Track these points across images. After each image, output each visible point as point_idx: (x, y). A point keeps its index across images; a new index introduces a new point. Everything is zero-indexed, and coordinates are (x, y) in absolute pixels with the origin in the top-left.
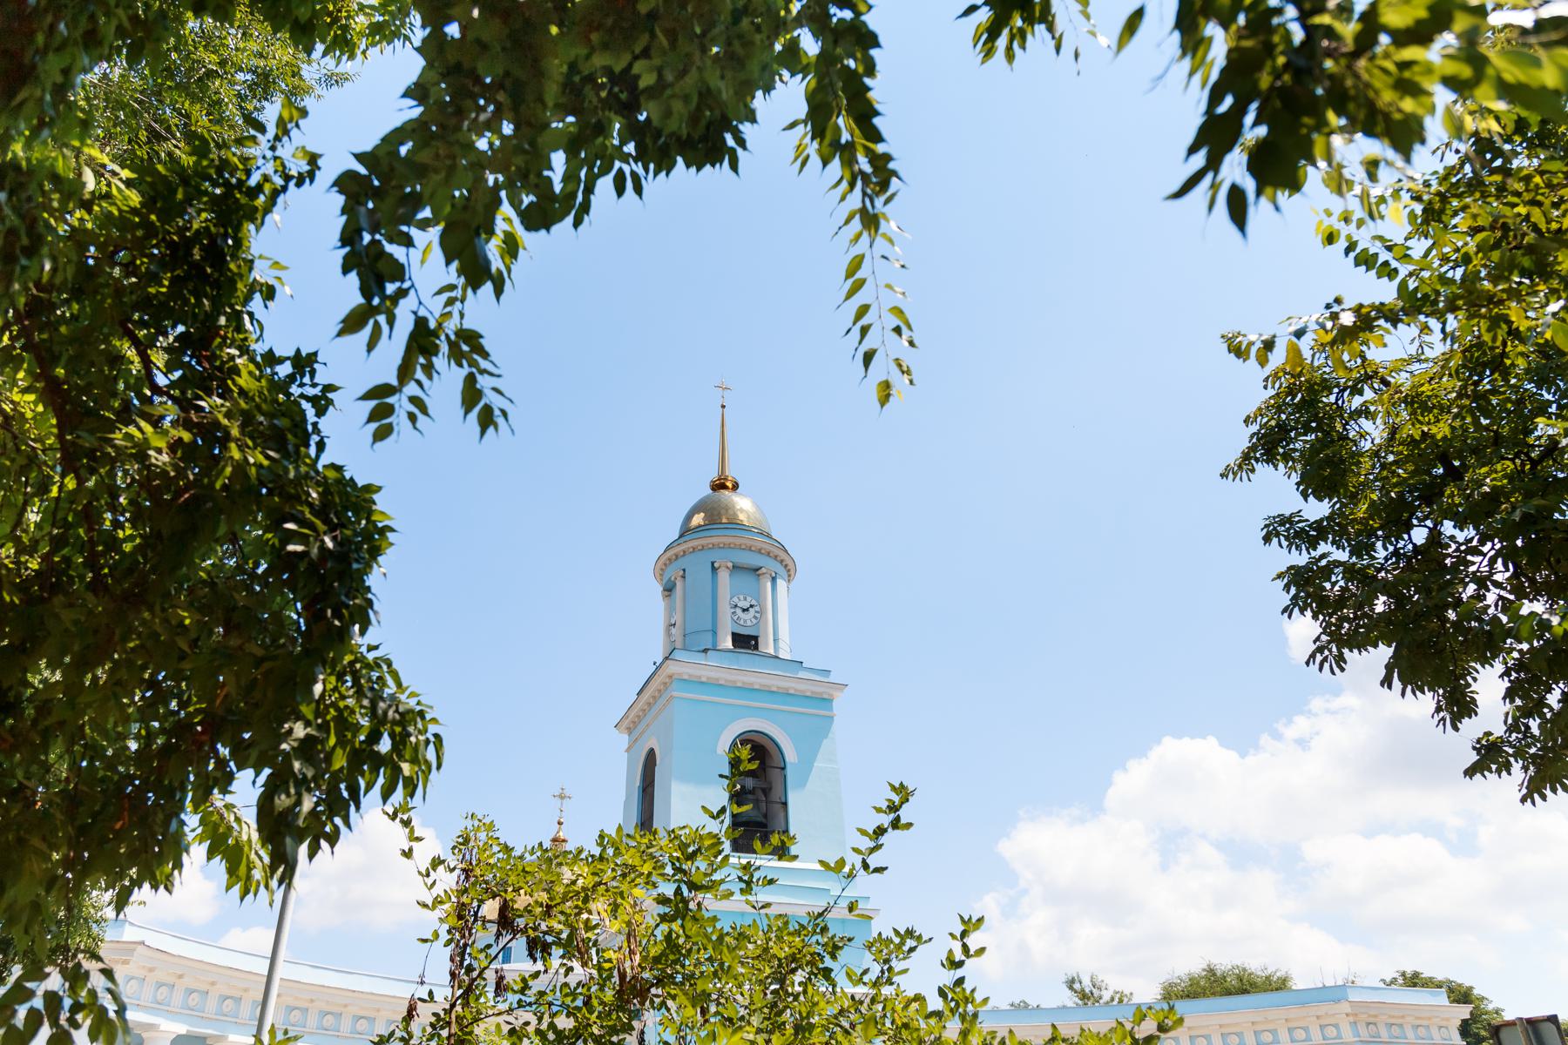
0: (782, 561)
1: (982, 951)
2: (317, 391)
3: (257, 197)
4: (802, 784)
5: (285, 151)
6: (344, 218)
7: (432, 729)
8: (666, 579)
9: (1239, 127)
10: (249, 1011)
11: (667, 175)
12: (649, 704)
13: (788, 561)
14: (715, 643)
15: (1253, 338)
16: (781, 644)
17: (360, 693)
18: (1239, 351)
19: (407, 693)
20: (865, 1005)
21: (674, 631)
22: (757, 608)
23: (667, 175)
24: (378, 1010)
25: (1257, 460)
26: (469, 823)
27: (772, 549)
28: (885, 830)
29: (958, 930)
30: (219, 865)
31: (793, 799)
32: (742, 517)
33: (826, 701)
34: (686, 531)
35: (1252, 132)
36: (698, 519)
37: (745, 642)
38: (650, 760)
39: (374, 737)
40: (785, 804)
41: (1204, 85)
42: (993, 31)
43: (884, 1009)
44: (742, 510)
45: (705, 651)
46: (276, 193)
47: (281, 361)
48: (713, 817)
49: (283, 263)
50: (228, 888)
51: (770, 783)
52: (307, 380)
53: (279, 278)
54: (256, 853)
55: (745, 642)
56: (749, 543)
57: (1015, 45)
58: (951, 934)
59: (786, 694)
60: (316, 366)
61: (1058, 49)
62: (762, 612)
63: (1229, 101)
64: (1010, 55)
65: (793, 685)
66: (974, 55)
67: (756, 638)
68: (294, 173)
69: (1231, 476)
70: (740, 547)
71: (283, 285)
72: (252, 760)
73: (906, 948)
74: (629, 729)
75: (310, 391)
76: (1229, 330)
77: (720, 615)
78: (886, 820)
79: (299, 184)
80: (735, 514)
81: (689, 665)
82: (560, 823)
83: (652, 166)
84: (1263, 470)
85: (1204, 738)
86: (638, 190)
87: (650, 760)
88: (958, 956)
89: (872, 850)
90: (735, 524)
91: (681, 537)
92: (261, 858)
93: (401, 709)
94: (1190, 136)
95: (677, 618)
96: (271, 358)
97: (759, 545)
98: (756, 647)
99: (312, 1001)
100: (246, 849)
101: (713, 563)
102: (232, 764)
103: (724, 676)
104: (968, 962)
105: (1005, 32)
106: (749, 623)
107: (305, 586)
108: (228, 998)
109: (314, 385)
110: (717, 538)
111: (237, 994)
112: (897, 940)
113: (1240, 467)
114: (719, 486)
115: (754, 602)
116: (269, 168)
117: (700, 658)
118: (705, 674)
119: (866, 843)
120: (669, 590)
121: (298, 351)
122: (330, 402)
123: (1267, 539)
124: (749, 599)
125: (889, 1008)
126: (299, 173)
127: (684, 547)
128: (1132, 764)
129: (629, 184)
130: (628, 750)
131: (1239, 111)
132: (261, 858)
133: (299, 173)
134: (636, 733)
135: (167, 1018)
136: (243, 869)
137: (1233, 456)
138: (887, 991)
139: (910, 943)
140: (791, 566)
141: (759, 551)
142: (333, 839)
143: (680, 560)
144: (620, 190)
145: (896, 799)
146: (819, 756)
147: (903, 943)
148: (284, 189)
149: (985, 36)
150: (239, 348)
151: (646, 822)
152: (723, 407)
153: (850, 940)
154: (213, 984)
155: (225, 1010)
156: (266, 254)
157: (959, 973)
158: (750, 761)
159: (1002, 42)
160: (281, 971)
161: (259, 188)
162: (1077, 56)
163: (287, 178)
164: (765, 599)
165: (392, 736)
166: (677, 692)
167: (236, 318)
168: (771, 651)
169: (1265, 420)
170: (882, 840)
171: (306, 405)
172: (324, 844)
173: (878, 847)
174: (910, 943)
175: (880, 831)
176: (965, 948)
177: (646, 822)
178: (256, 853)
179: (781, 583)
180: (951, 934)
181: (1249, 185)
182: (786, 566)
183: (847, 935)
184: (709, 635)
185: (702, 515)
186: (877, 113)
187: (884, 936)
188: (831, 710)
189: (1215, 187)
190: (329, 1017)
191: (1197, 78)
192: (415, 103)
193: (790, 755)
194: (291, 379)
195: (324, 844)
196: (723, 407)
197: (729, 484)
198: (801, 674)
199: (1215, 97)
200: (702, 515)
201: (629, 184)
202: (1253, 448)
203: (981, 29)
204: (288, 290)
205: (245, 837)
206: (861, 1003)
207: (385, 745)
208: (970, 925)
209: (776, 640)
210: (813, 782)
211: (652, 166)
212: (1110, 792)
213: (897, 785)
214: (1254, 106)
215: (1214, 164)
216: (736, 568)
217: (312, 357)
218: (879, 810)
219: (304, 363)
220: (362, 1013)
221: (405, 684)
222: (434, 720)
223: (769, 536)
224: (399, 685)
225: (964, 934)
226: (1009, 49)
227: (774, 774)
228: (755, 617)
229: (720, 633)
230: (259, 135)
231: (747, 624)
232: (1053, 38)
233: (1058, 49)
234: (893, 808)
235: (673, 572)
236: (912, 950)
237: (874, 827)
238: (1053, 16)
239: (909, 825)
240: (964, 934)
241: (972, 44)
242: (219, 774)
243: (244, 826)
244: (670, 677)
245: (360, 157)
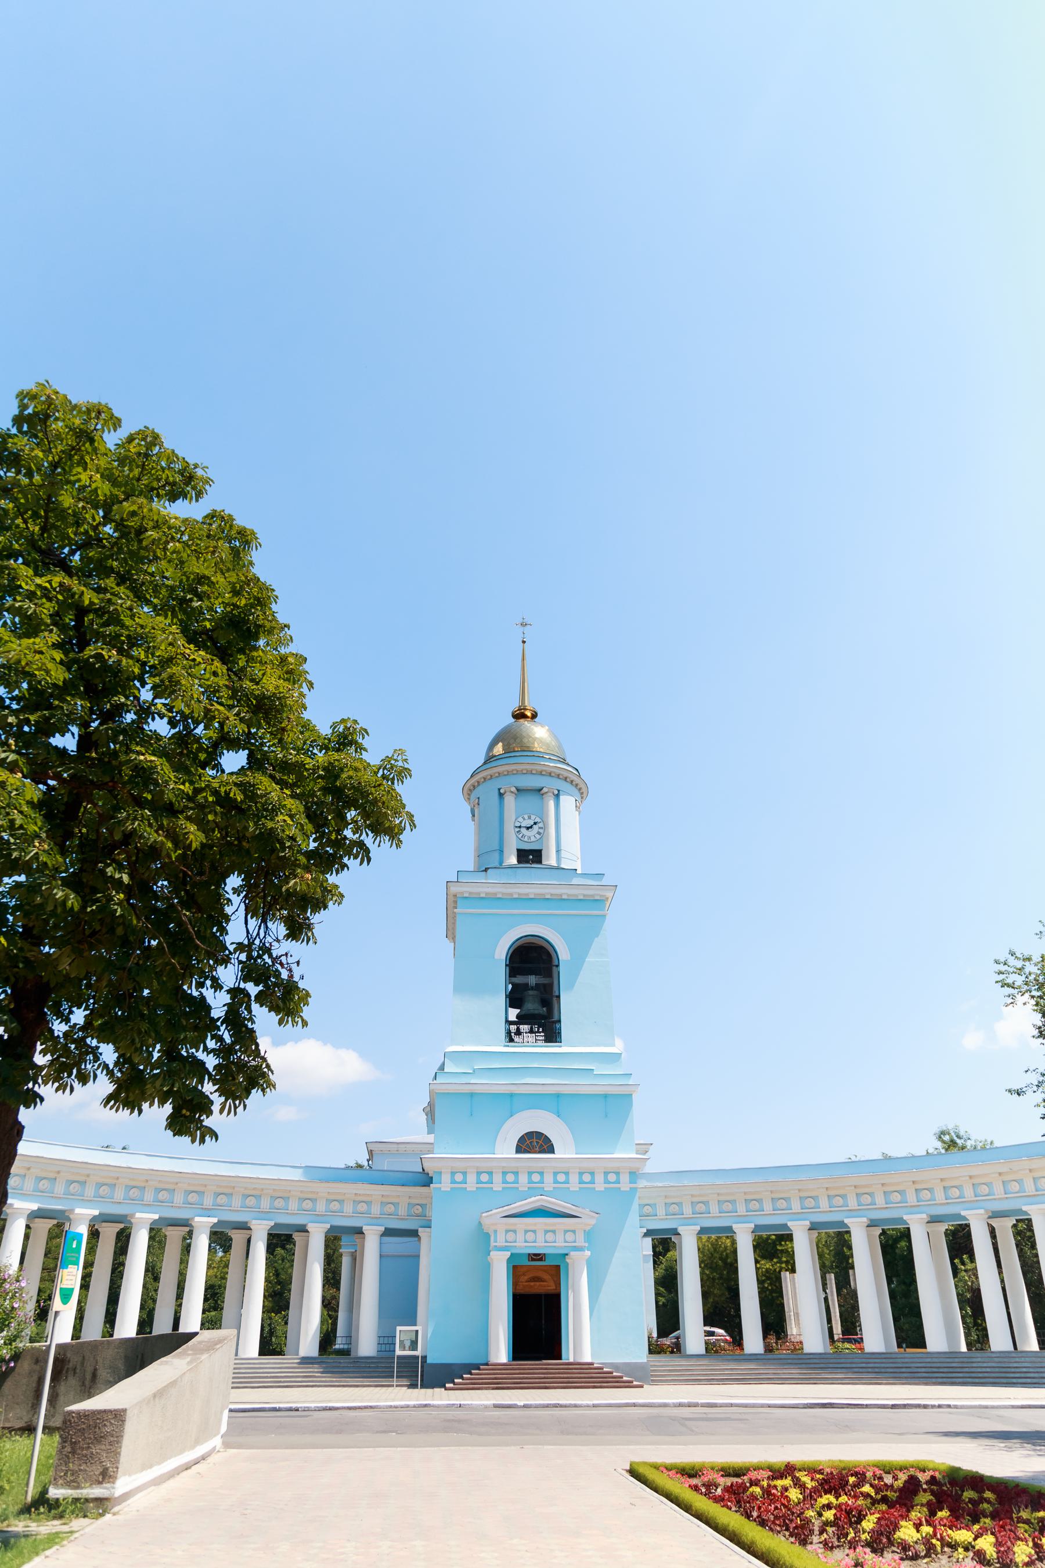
4: (571, 986)
13: (582, 785)
22: (541, 825)
24: (118, 1178)
27: (561, 772)
32: (537, 747)
33: (599, 902)
34: (490, 759)
37: (530, 856)
40: (559, 997)
55: (530, 856)
56: (539, 768)
59: (560, 900)
62: (545, 828)
70: (531, 772)
91: (485, 763)
98: (540, 862)
99: (147, 1181)
101: (499, 789)
103: (499, 890)
106: (533, 839)
114: (519, 715)
115: (538, 820)
118: (483, 890)
122: (202, 1141)
124: (533, 817)
135: (19, 1199)
140: (584, 790)
143: (568, 785)
146: (591, 952)
152: (524, 642)
164: (547, 816)
168: (553, 862)
182: (580, 789)
184: (497, 855)
185: (500, 744)
190: (43, 1182)
196: (524, 642)
197: (529, 714)
198: (575, 881)
200: (500, 744)
209: (558, 851)
220: (221, 1190)
228: (539, 833)
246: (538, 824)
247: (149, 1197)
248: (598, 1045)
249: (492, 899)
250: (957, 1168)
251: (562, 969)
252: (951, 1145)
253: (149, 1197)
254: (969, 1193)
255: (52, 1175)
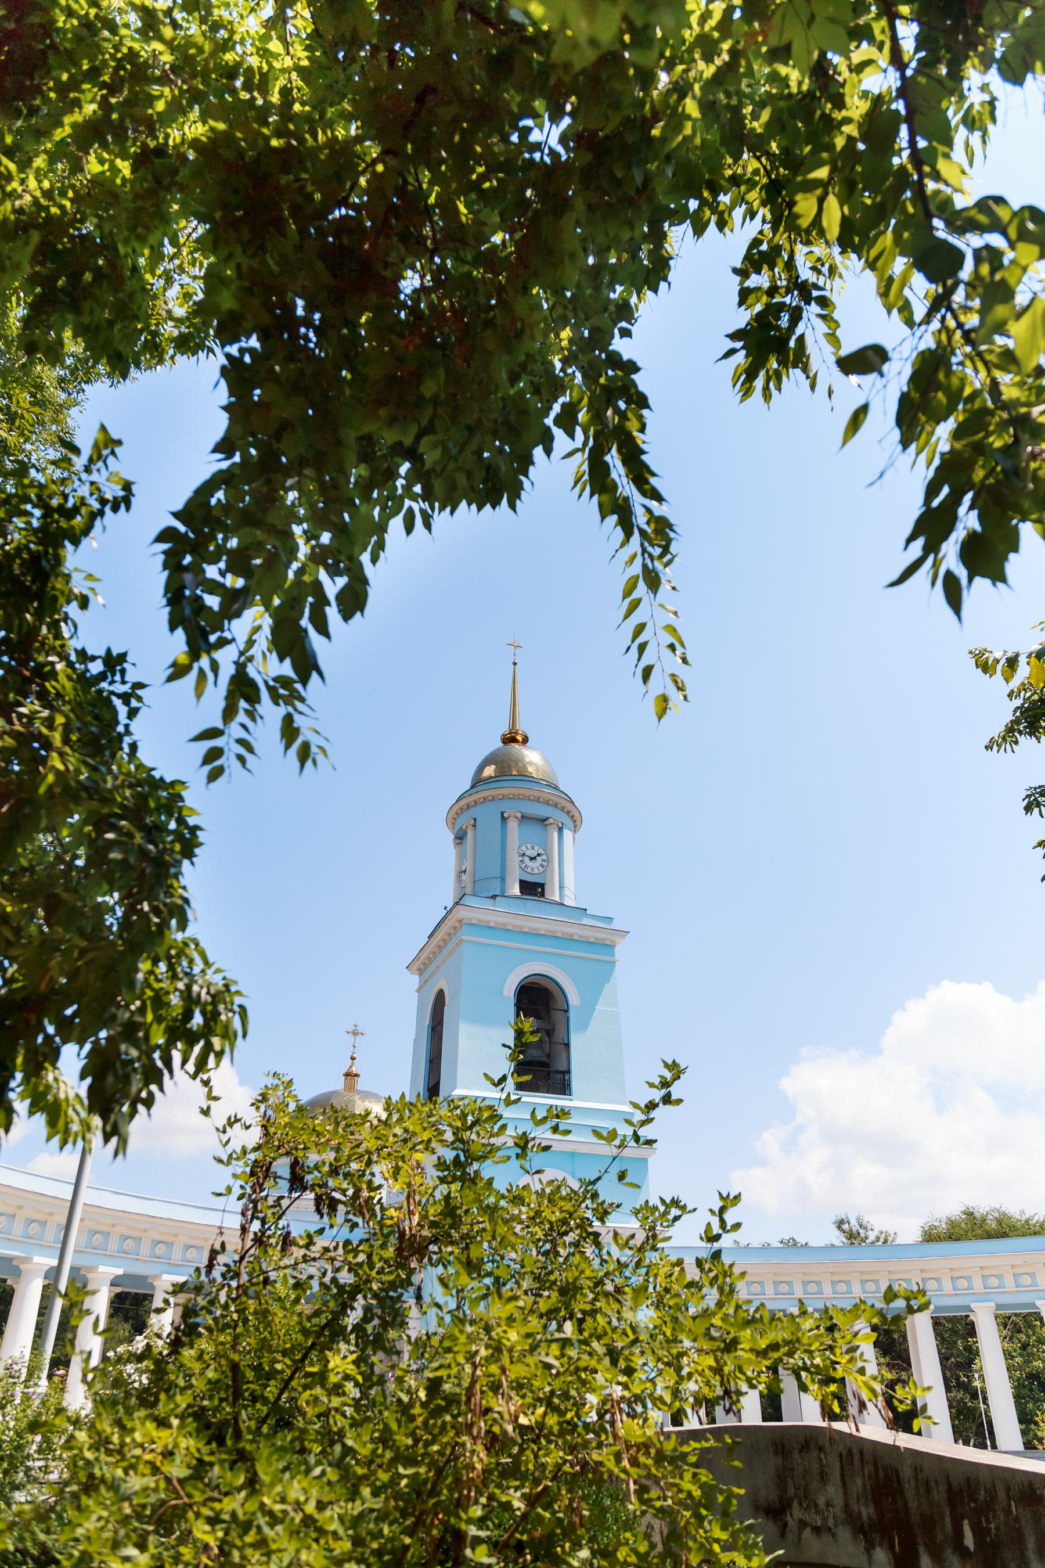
0: (568, 812)
1: (737, 1226)
2: (126, 688)
3: (74, 517)
4: (584, 1027)
5: (99, 477)
6: (166, 573)
7: (238, 1000)
8: (457, 828)
9: (954, 518)
10: (53, 1235)
11: (452, 513)
12: (439, 947)
14: (503, 891)
15: (998, 654)
16: (566, 891)
17: (174, 977)
18: (985, 667)
19: (213, 969)
20: (630, 1268)
21: (464, 877)
22: (544, 857)
23: (452, 513)
25: (1020, 733)
26: (270, 1081)
28: (657, 1105)
29: (717, 1205)
30: (40, 1120)
31: (576, 1041)
32: (531, 769)
33: (609, 947)
34: (478, 781)
35: (968, 520)
36: (489, 771)
37: (532, 889)
38: (440, 1000)
39: (188, 1015)
40: (567, 1045)
41: (929, 464)
42: (751, 374)
43: (647, 1274)
44: (531, 763)
45: (494, 897)
46: (93, 516)
47: (93, 658)
48: (496, 1085)
49: (96, 575)
50: (48, 1139)
51: (554, 1025)
52: (118, 678)
53: (92, 589)
54: (74, 1110)
55: (532, 889)
56: (537, 794)
57: (772, 385)
58: (711, 1210)
59: (570, 939)
60: (125, 665)
61: (813, 387)
62: (549, 860)
63: (946, 490)
64: (767, 395)
65: (577, 931)
66: (733, 395)
67: (542, 886)
68: (109, 496)
69: (995, 748)
71: (96, 594)
72: (76, 1032)
73: (671, 1217)
74: (419, 970)
75: (120, 688)
76: (978, 645)
77: (508, 863)
78: (657, 1095)
79: (115, 509)
80: (525, 768)
81: (478, 910)
82: (353, 1059)
83: (437, 504)
84: (1025, 742)
85: (980, 984)
86: (428, 526)
87: (440, 1000)
88: (716, 1229)
89: (643, 1123)
90: (524, 776)
91: (472, 787)
92: (78, 1113)
93: (212, 991)
94: (908, 529)
95: (468, 865)
96: (83, 656)
97: (547, 797)
98: (542, 894)
100: (64, 1104)
102: (57, 1039)
103: (511, 921)
104: (724, 1236)
105: (762, 374)
107: (121, 877)
108: (34, 1221)
109: (124, 682)
110: (508, 788)
111: (42, 1217)
112: (662, 1208)
113: (1004, 739)
114: (510, 739)
116: (84, 491)
117: (488, 904)
118: (493, 919)
119: (639, 1116)
120: (460, 838)
121: (109, 651)
123: (1028, 809)
125: (651, 1274)
126: (115, 498)
127: (475, 797)
128: (910, 1004)
129: (418, 520)
130: (418, 991)
131: (954, 500)
132: (78, 1113)
133: (115, 498)
134: (426, 976)
136: (61, 1124)
137: (998, 728)
138: (651, 1257)
139: (674, 1212)
141: (547, 802)
142: (149, 1102)
143: (471, 810)
144: (409, 528)
145: (668, 1075)
147: (666, 1213)
148: (101, 513)
149: (743, 377)
150: (59, 655)
151: (433, 1090)
152: (515, 664)
153: (618, 1206)
154: (20, 1207)
155: (31, 1232)
156: (80, 567)
157: (716, 1245)
158: (532, 1033)
159: (759, 383)
160: (86, 1196)
161: (76, 510)
162: (830, 393)
163: (103, 502)
164: (552, 849)
165: (203, 1013)
166: (466, 935)
167: (55, 627)
168: (557, 898)
169: (1028, 694)
170: (653, 1114)
171: (117, 702)
172: (141, 1108)
173: (649, 1121)
174: (674, 1212)
175: (651, 1106)
176: (722, 1222)
177: (433, 1090)
178: (74, 1110)
179: (567, 834)
180: (711, 1210)
181: (962, 573)
183: (616, 1202)
184: (498, 882)
185: (493, 767)
186: (644, 452)
187: (651, 1204)
188: (613, 954)
189: (936, 565)
191: (923, 457)
192: (222, 456)
193: (574, 999)
194: (102, 677)
195: (141, 1108)
196: (515, 664)
197: (519, 738)
198: (585, 921)
199: (932, 490)
200: (493, 767)
201: (418, 520)
202: (1016, 722)
203: (740, 371)
204: (100, 600)
205: (62, 1096)
206: (626, 1266)
207: (198, 1020)
208: (729, 1201)
209: (561, 888)
210: (594, 1025)
211: (437, 504)
212: (890, 1031)
213: (670, 1062)
214: (969, 495)
215: (932, 548)
216: (525, 818)
217: (122, 657)
218: (651, 1085)
219: (114, 662)
220: (192, 1242)
221: (211, 961)
222: (238, 993)
223: (556, 788)
224: (207, 963)
225: (722, 1210)
226: (766, 389)
227: (558, 1016)
229: (508, 880)
230: (74, 457)
231: (534, 871)
232: (808, 377)
233: (813, 387)
234: (665, 1084)
235: (464, 821)
236: (676, 1219)
237: (647, 1101)
238: (808, 357)
239: (679, 1101)
240: (722, 1210)
241: (731, 384)
242: (47, 1050)
243: (62, 1085)
244: (460, 921)
245: (176, 515)
246: (544, 856)
247: (113, 1244)
248: (611, 1102)
249: (502, 929)
250: (863, 1259)
251: (573, 1015)
252: (852, 1236)
253: (113, 1244)
254: (978, 1285)
255: (11, 1211)
